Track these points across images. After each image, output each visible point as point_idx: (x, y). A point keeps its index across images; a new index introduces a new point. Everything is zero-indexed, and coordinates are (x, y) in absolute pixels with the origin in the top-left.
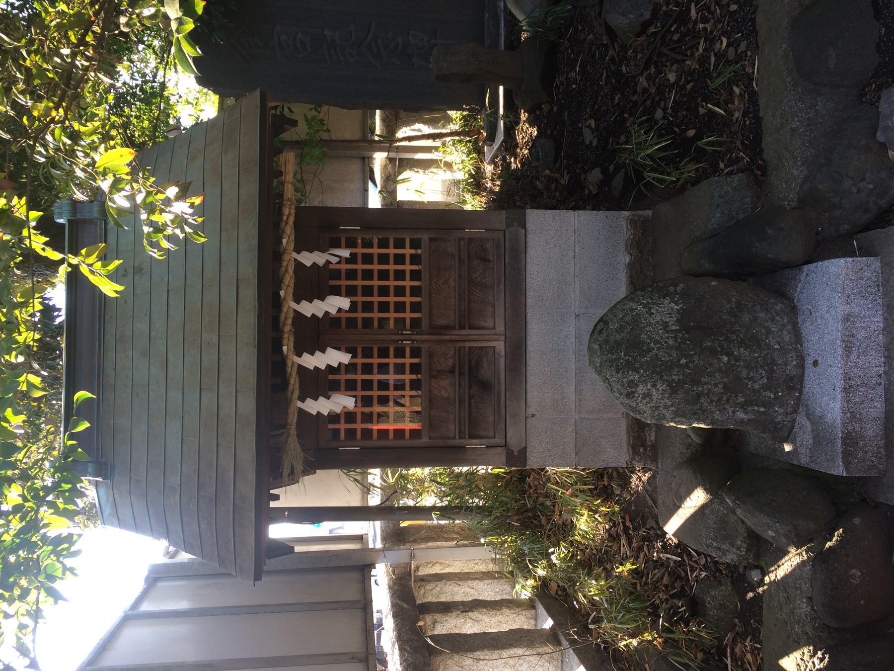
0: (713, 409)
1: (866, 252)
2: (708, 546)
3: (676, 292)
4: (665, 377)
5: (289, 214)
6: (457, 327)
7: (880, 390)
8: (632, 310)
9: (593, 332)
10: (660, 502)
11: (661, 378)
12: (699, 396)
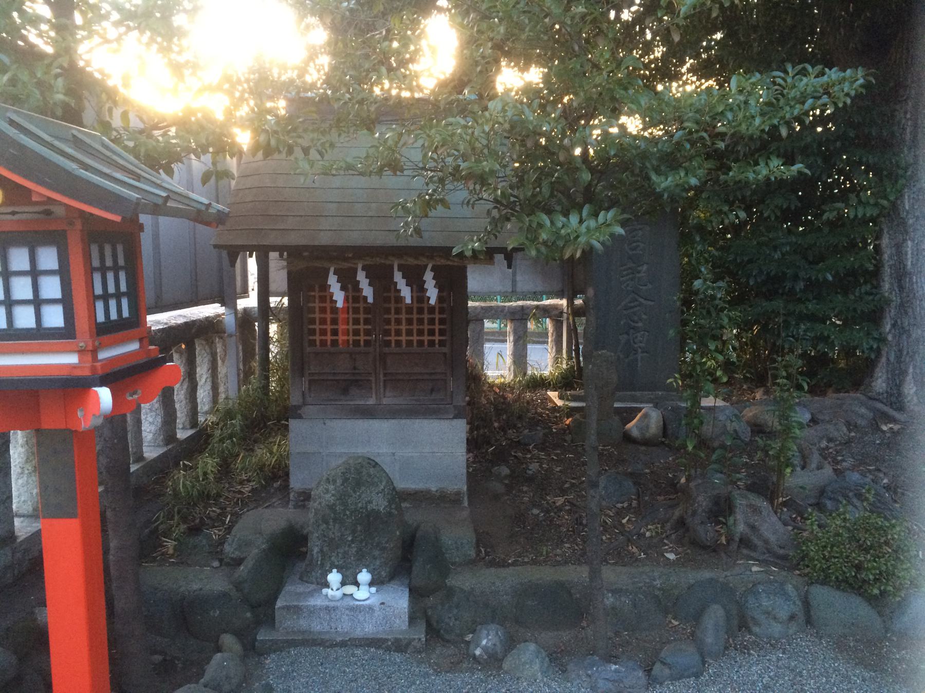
0: (319, 532)
1: (412, 619)
2: (235, 536)
3: (391, 509)
4: (338, 502)
5: (454, 261)
6: (385, 372)
7: (327, 628)
8: (381, 482)
9: (369, 459)
10: (266, 510)
11: (338, 499)
12: (327, 523)
